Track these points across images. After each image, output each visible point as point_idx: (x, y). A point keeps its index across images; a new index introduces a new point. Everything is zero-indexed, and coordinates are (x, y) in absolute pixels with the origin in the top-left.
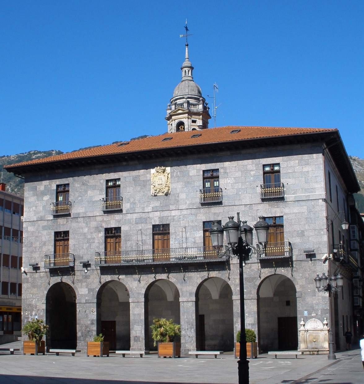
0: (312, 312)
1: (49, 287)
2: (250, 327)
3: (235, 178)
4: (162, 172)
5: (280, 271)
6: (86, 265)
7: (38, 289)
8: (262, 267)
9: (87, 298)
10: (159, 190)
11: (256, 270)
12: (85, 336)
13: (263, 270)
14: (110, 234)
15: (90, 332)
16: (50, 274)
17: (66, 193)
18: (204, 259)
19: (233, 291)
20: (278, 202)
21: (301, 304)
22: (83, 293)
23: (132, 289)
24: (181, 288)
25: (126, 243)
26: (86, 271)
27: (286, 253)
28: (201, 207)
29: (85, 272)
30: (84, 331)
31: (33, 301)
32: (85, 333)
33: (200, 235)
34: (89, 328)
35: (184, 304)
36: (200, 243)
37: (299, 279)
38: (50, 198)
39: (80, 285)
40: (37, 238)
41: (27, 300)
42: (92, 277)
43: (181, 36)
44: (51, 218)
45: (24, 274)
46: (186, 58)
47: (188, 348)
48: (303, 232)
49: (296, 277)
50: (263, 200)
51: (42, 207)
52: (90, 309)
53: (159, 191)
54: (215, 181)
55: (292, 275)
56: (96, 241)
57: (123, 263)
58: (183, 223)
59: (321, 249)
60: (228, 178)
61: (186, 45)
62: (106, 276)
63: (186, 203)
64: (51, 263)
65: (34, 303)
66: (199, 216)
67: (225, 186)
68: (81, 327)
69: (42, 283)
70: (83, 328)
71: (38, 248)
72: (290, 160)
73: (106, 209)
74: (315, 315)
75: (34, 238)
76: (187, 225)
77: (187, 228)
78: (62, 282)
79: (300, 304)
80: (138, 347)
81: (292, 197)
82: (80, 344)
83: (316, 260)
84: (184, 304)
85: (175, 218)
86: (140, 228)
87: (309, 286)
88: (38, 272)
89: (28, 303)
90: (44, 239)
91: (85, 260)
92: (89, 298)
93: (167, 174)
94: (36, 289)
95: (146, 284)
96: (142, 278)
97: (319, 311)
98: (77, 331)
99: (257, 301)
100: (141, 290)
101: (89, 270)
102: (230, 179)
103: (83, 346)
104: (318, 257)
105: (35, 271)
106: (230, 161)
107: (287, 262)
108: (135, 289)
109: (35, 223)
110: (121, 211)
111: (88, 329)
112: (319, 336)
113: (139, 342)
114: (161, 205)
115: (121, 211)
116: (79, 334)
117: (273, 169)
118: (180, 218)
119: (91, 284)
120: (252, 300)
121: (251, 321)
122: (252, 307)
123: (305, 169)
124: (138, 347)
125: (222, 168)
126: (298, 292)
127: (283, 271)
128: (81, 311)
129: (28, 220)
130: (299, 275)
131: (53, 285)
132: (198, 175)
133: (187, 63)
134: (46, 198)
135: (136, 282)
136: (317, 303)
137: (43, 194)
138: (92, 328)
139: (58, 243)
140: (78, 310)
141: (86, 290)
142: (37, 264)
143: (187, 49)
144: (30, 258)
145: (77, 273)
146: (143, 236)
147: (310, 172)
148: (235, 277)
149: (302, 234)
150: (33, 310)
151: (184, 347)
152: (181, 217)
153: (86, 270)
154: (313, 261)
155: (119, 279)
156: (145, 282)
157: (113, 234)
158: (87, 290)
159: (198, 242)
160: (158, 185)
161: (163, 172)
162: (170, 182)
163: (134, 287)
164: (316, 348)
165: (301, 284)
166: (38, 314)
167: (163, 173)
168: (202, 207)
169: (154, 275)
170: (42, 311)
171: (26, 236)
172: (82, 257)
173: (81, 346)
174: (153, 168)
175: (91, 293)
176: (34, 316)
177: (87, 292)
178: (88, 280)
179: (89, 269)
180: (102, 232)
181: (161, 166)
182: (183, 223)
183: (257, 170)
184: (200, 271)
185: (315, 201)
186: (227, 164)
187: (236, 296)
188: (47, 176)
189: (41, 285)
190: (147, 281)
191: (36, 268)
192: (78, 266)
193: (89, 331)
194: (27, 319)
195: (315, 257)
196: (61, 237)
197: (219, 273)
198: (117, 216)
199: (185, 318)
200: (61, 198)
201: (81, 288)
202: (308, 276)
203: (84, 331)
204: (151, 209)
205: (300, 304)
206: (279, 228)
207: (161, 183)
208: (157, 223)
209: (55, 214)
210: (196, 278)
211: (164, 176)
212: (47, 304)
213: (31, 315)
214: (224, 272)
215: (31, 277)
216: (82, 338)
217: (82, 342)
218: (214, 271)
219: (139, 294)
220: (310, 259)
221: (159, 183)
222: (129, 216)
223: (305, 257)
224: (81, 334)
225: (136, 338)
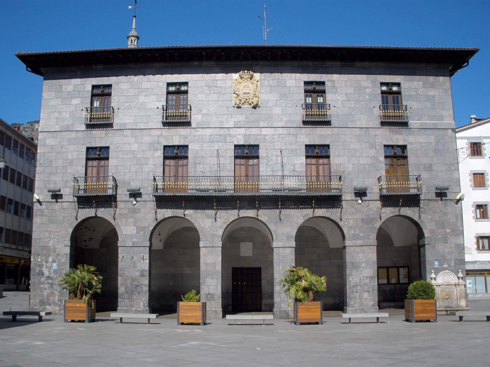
0: (444, 262)
1: (76, 223)
2: (368, 281)
3: (347, 95)
4: (249, 79)
5: (404, 211)
6: (135, 194)
7: (58, 226)
8: (384, 205)
9: (134, 240)
10: (245, 100)
11: (375, 209)
12: (130, 293)
13: (384, 210)
14: (183, 154)
15: (138, 288)
16: (78, 205)
17: (105, 97)
18: (84, 192)
19: (345, 235)
20: (400, 127)
21: (431, 252)
22: (128, 233)
23: (203, 229)
24: (276, 230)
25: (195, 167)
26: (134, 202)
27: (411, 189)
28: (302, 126)
29: (133, 203)
30: (129, 285)
31: (50, 242)
32: (131, 289)
33: (301, 162)
34: (137, 282)
35: (279, 251)
36: (302, 172)
37: (428, 222)
38: (82, 102)
39: (124, 221)
40: (60, 155)
41: (40, 241)
42: (143, 211)
43: (130, 7)
44: (83, 127)
45: (38, 204)
46: (133, 28)
47: (284, 310)
48: (430, 165)
49: (424, 220)
50: (383, 124)
51: (68, 113)
52: (139, 255)
53: (245, 102)
54: (318, 96)
55: (420, 217)
56: (151, 162)
57: (190, 193)
58: (278, 146)
59: (452, 187)
60: (337, 93)
61: (134, 16)
62: (164, 210)
63: (282, 120)
65: (51, 245)
66: (300, 137)
67: (334, 103)
68: (126, 280)
69: (64, 217)
70: (129, 281)
71: (61, 168)
72: (413, 80)
73: (166, 120)
74: (447, 266)
75: (55, 154)
76: (283, 148)
77: (283, 153)
78: (96, 217)
79: (429, 253)
80: (211, 308)
81: (417, 123)
82: (122, 304)
83: (446, 200)
84: (279, 251)
85: (267, 137)
86: (217, 148)
87: (440, 231)
88: (60, 202)
89: (41, 244)
90: (70, 156)
91: (134, 186)
92: (137, 240)
93: (256, 82)
94: (55, 225)
95: (225, 223)
96: (218, 214)
97: (453, 261)
98: (119, 286)
99: (377, 248)
100: (217, 231)
101: (138, 201)
102: (340, 95)
103: (128, 306)
104: (449, 196)
105: (54, 200)
106: (340, 74)
107: (413, 200)
108: (208, 229)
109: (57, 135)
110: (188, 124)
112: (453, 292)
113: (213, 302)
114: (247, 120)
115: (188, 124)
116: (121, 290)
117: (390, 89)
118: (274, 138)
120: (371, 246)
121: (369, 273)
122: (370, 255)
123: (431, 93)
124: (211, 308)
125: (328, 81)
126: (427, 237)
127: (408, 211)
128: (125, 257)
129: (46, 130)
130: (427, 218)
132: (298, 87)
133: (133, 33)
134: (75, 102)
135: (210, 220)
136: (449, 251)
137: (71, 96)
138: (143, 281)
139: (90, 163)
140: (120, 256)
141: (134, 229)
142: (60, 191)
143: (134, 19)
144: (47, 182)
145: (120, 205)
146: (221, 159)
147: (436, 97)
148: (348, 218)
149: (429, 168)
150: (50, 255)
151: (279, 307)
152: (275, 137)
153: (134, 201)
154: (443, 201)
155: (184, 215)
156: (223, 220)
157: (176, 154)
158: (135, 228)
159: (298, 170)
160: (244, 93)
161: (251, 78)
162: (259, 91)
163: (207, 227)
164: (451, 307)
165: (430, 228)
166: (57, 261)
167: (250, 80)
168: (304, 126)
169: (236, 211)
170: (65, 256)
171: (42, 151)
172: (129, 184)
173: (125, 307)
174: (236, 72)
175: (142, 233)
176: (50, 263)
177: (135, 231)
178: (138, 216)
179: (138, 199)
180: (159, 151)
181: (248, 70)
182: (277, 145)
183: (373, 87)
184: (302, 208)
185: (444, 131)
186: (335, 77)
187: (350, 241)
188: (79, 73)
189: (64, 220)
190: (226, 219)
191: (56, 196)
192: (122, 195)
193: (137, 286)
194: (40, 268)
195: (446, 196)
196: (97, 155)
197: (327, 211)
198: (182, 131)
199: (280, 269)
200: (96, 104)
201: (126, 225)
202: (438, 219)
203: (129, 285)
204: (233, 124)
205: (429, 253)
206: (400, 159)
207: (248, 92)
208: (242, 143)
209: (88, 122)
210: (297, 217)
211: (252, 83)
212: (71, 246)
213: (47, 262)
214: (334, 210)
215: (47, 208)
216: (126, 295)
217: (126, 301)
218: (321, 208)
219: (213, 236)
220: (440, 198)
221: (244, 91)
222: (200, 132)
223: (435, 196)
224: (124, 289)
225: (209, 296)
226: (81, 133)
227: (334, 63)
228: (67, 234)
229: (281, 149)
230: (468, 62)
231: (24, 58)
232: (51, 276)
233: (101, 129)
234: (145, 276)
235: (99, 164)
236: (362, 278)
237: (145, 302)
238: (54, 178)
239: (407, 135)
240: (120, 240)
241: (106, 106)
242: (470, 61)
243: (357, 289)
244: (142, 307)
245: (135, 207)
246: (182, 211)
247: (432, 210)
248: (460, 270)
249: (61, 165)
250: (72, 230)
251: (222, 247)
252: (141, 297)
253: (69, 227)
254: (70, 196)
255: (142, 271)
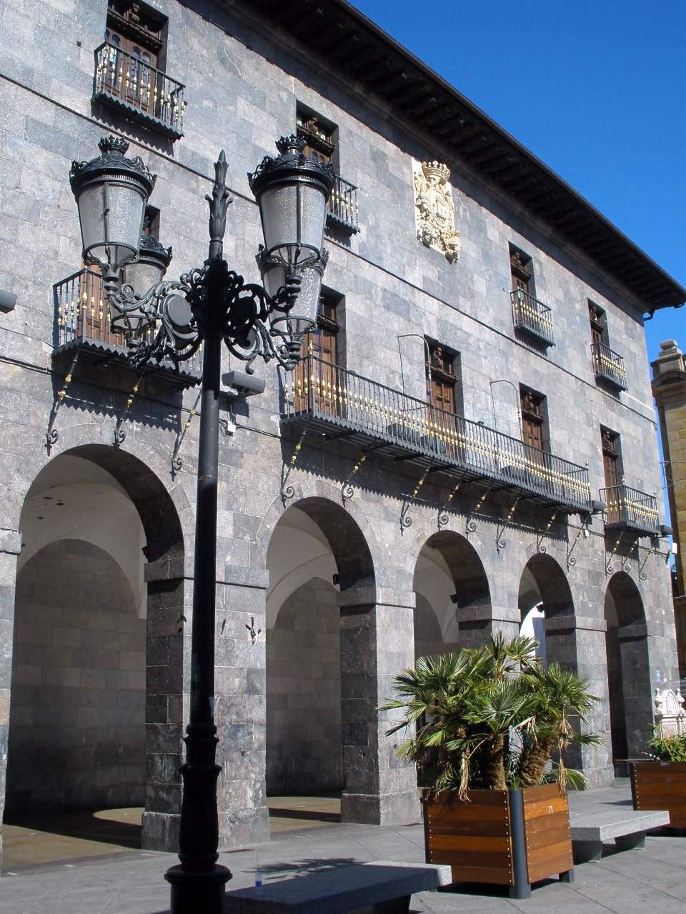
1: (44, 459)
34: (238, 714)
42: (248, 461)
52: (240, 614)
62: (88, 416)
64: (62, 327)
111: (234, 717)
119: (246, 494)
131: (132, 456)
135: (392, 525)
158: (231, 519)
184: (524, 530)
193: (237, 727)
226: (74, 119)
228: (9, 498)
230: (651, 313)
233: (137, 139)
234: (257, 692)
237: (258, 785)
242: (656, 311)
244: (251, 804)
245: (231, 444)
246: (339, 485)
250: (26, 486)
251: (606, 632)
252: (246, 768)
253: (18, 470)
254: (26, 342)
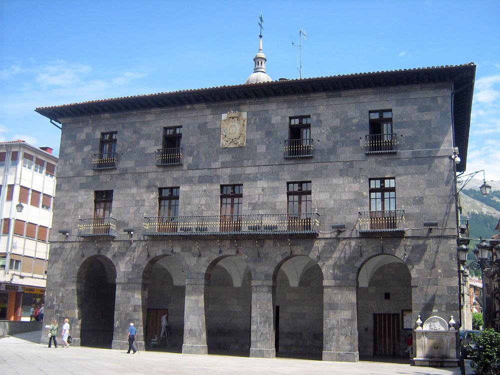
56: (147, 204)
70: (123, 316)
74: (437, 311)
100: (201, 269)
126: (414, 279)
134: (87, 149)
156: (206, 258)
227: (319, 95)
229: (263, 188)
231: (43, 112)
232: (60, 309)
235: (233, 201)
236: (339, 320)
238: (67, 220)
239: (396, 167)
240: (118, 277)
241: (111, 152)
243: (334, 332)
247: (421, 248)
248: (452, 316)
249: (73, 208)
255: (135, 306)
